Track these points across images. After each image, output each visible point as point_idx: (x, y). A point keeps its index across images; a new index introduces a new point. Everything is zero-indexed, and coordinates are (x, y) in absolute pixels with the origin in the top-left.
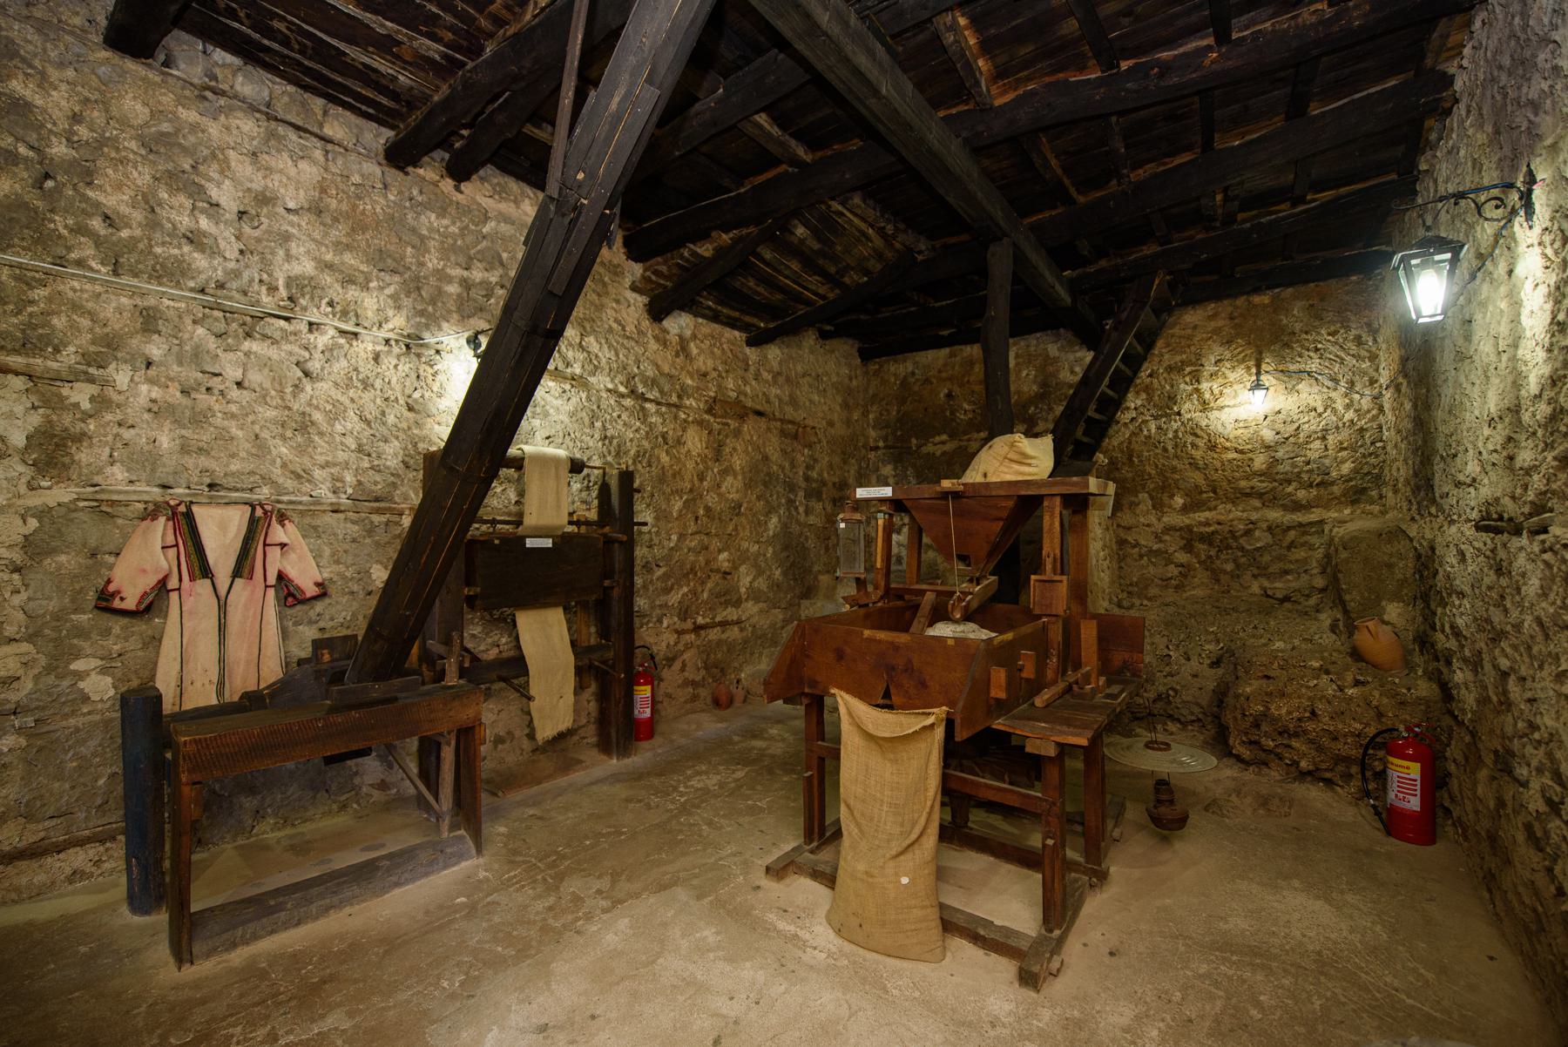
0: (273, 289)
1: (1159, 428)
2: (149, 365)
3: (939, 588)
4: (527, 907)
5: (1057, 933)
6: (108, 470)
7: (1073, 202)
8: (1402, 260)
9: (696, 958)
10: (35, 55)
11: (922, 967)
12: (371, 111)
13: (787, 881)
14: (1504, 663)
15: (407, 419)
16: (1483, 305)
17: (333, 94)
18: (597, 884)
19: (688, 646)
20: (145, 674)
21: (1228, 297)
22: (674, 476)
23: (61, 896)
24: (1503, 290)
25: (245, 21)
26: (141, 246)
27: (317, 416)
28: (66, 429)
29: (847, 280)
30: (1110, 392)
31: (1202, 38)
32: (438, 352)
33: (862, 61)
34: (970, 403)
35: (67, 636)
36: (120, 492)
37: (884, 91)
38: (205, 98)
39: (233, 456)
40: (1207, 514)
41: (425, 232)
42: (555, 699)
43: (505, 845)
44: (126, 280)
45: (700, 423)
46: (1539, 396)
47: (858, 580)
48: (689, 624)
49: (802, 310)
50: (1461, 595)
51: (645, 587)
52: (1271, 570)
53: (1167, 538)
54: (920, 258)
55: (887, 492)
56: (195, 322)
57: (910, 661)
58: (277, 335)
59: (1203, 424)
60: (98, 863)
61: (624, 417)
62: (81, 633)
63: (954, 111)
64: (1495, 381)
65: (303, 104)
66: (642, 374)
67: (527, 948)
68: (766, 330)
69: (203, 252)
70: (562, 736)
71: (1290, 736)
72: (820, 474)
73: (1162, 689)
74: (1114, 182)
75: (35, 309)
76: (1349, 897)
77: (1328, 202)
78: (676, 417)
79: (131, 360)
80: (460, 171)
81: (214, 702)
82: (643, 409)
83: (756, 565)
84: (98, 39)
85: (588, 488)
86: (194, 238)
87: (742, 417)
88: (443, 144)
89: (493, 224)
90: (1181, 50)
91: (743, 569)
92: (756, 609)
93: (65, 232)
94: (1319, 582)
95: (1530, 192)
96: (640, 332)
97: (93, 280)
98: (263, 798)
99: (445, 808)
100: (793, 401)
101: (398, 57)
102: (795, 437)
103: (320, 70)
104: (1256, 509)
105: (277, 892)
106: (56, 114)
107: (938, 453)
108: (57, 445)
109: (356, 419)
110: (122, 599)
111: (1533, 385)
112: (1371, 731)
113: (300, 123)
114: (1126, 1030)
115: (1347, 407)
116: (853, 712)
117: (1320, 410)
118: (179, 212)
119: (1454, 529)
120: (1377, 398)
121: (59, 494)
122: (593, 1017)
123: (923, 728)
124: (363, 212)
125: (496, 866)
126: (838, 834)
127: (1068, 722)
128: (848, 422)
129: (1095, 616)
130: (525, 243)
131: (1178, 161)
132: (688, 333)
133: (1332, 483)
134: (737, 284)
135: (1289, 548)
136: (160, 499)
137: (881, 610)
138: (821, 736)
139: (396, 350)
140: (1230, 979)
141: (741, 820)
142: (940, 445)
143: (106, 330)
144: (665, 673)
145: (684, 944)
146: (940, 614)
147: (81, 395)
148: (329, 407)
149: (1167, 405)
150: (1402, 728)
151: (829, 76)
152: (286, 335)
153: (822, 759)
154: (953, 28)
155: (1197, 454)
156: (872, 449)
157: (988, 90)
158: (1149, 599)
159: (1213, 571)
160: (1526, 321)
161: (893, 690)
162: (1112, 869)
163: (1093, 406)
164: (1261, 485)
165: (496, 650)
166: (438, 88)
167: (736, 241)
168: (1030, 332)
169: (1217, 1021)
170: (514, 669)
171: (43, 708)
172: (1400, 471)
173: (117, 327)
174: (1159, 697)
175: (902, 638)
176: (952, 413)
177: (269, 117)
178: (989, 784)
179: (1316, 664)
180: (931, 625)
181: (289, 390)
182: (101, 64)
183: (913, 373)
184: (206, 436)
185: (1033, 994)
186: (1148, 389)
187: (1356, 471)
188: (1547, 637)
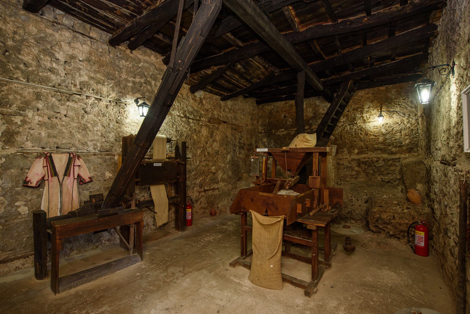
0: (75, 86)
1: (350, 128)
2: (38, 110)
3: (282, 179)
4: (158, 276)
5: (316, 281)
6: (26, 143)
7: (324, 59)
8: (417, 85)
9: (210, 289)
10: (2, 13)
11: (276, 291)
12: (105, 29)
13: (236, 267)
14: (446, 203)
15: (116, 126)
16: (443, 97)
17: (93, 23)
18: (179, 269)
19: (202, 196)
20: (38, 206)
21: (372, 87)
22: (198, 143)
23: (12, 275)
24: (447, 94)
25: (68, 2)
26: (35, 73)
27: (89, 125)
28: (14, 130)
29: (253, 81)
30: (335, 117)
31: (363, 13)
32: (125, 104)
33: (261, 22)
34: (292, 119)
35: (15, 194)
36: (29, 150)
37: (267, 30)
38: (54, 25)
39: (64, 138)
40: (365, 155)
41: (122, 67)
42: (163, 213)
43: (149, 258)
44: (31, 83)
45: (206, 126)
46: (454, 127)
47: (257, 177)
48: (202, 190)
49: (239, 90)
50: (437, 182)
51: (189, 178)
52: (384, 173)
53: (352, 162)
54: (276, 74)
55: (266, 150)
56: (52, 96)
57: (273, 202)
58: (77, 100)
59: (364, 127)
60: (23, 265)
61: (183, 124)
62: (18, 193)
63: (287, 32)
64: (445, 120)
65: (84, 27)
66: (188, 110)
67: (160, 288)
68: (227, 96)
69: (54, 74)
70: (164, 225)
71: (387, 224)
72: (244, 141)
73: (350, 210)
74: (336, 53)
75: (4, 93)
76: (402, 272)
77: (402, 60)
78: (199, 124)
79: (33, 109)
80: (132, 47)
81: (59, 214)
82: (188, 121)
83: (223, 170)
84: (21, 7)
85: (171, 147)
86: (51, 70)
87: (219, 124)
88: (129, 39)
89: (142, 63)
90: (356, 17)
91: (219, 172)
92: (223, 184)
93: (12, 69)
94: (399, 177)
95: (453, 67)
96: (188, 97)
97: (21, 84)
98: (73, 244)
99: (131, 247)
100: (235, 118)
101: (115, 14)
102: (236, 130)
103: (90, 17)
104: (380, 154)
105: (82, 272)
106: (9, 32)
107: (281, 135)
108: (11, 135)
109: (101, 126)
110: (31, 183)
111: (453, 124)
112: (411, 223)
113: (83, 33)
114: (335, 308)
115: (408, 122)
116: (257, 218)
117: (400, 123)
118: (47, 62)
119: (435, 163)
120: (417, 120)
121: (11, 151)
122: (182, 306)
123: (277, 222)
124: (103, 61)
125: (147, 264)
126: (251, 253)
127: (320, 220)
128: (252, 124)
129: (329, 188)
130: (162, 79)
131: (356, 48)
132: (202, 97)
133: (403, 146)
134: (218, 82)
135: (390, 166)
136: (41, 152)
137: (264, 186)
138: (246, 224)
139: (113, 104)
140: (365, 294)
141: (221, 250)
142: (282, 132)
143: (25, 99)
144: (195, 205)
145: (207, 285)
146: (282, 187)
147: (18, 120)
148: (92, 122)
149: (353, 121)
150: (419, 222)
151: (251, 26)
152: (79, 100)
153: (246, 231)
154: (288, 10)
155: (362, 136)
156: (260, 133)
157: (298, 27)
158: (347, 182)
159: (366, 173)
160: (452, 105)
161: (268, 210)
162: (333, 264)
163: (330, 121)
164: (381, 146)
165: (143, 198)
166: (127, 23)
167: (219, 69)
168: (310, 97)
169: (361, 305)
170: (149, 204)
171: (7, 217)
172: (423, 143)
173: (28, 98)
174: (348, 213)
175: (271, 195)
176: (286, 122)
177: (74, 31)
178: (296, 238)
179: (395, 202)
180: (279, 190)
181: (80, 117)
182: (23, 15)
183: (273, 109)
184: (55, 132)
185: (309, 298)
186: (347, 116)
187: (410, 142)
188: (455, 196)
